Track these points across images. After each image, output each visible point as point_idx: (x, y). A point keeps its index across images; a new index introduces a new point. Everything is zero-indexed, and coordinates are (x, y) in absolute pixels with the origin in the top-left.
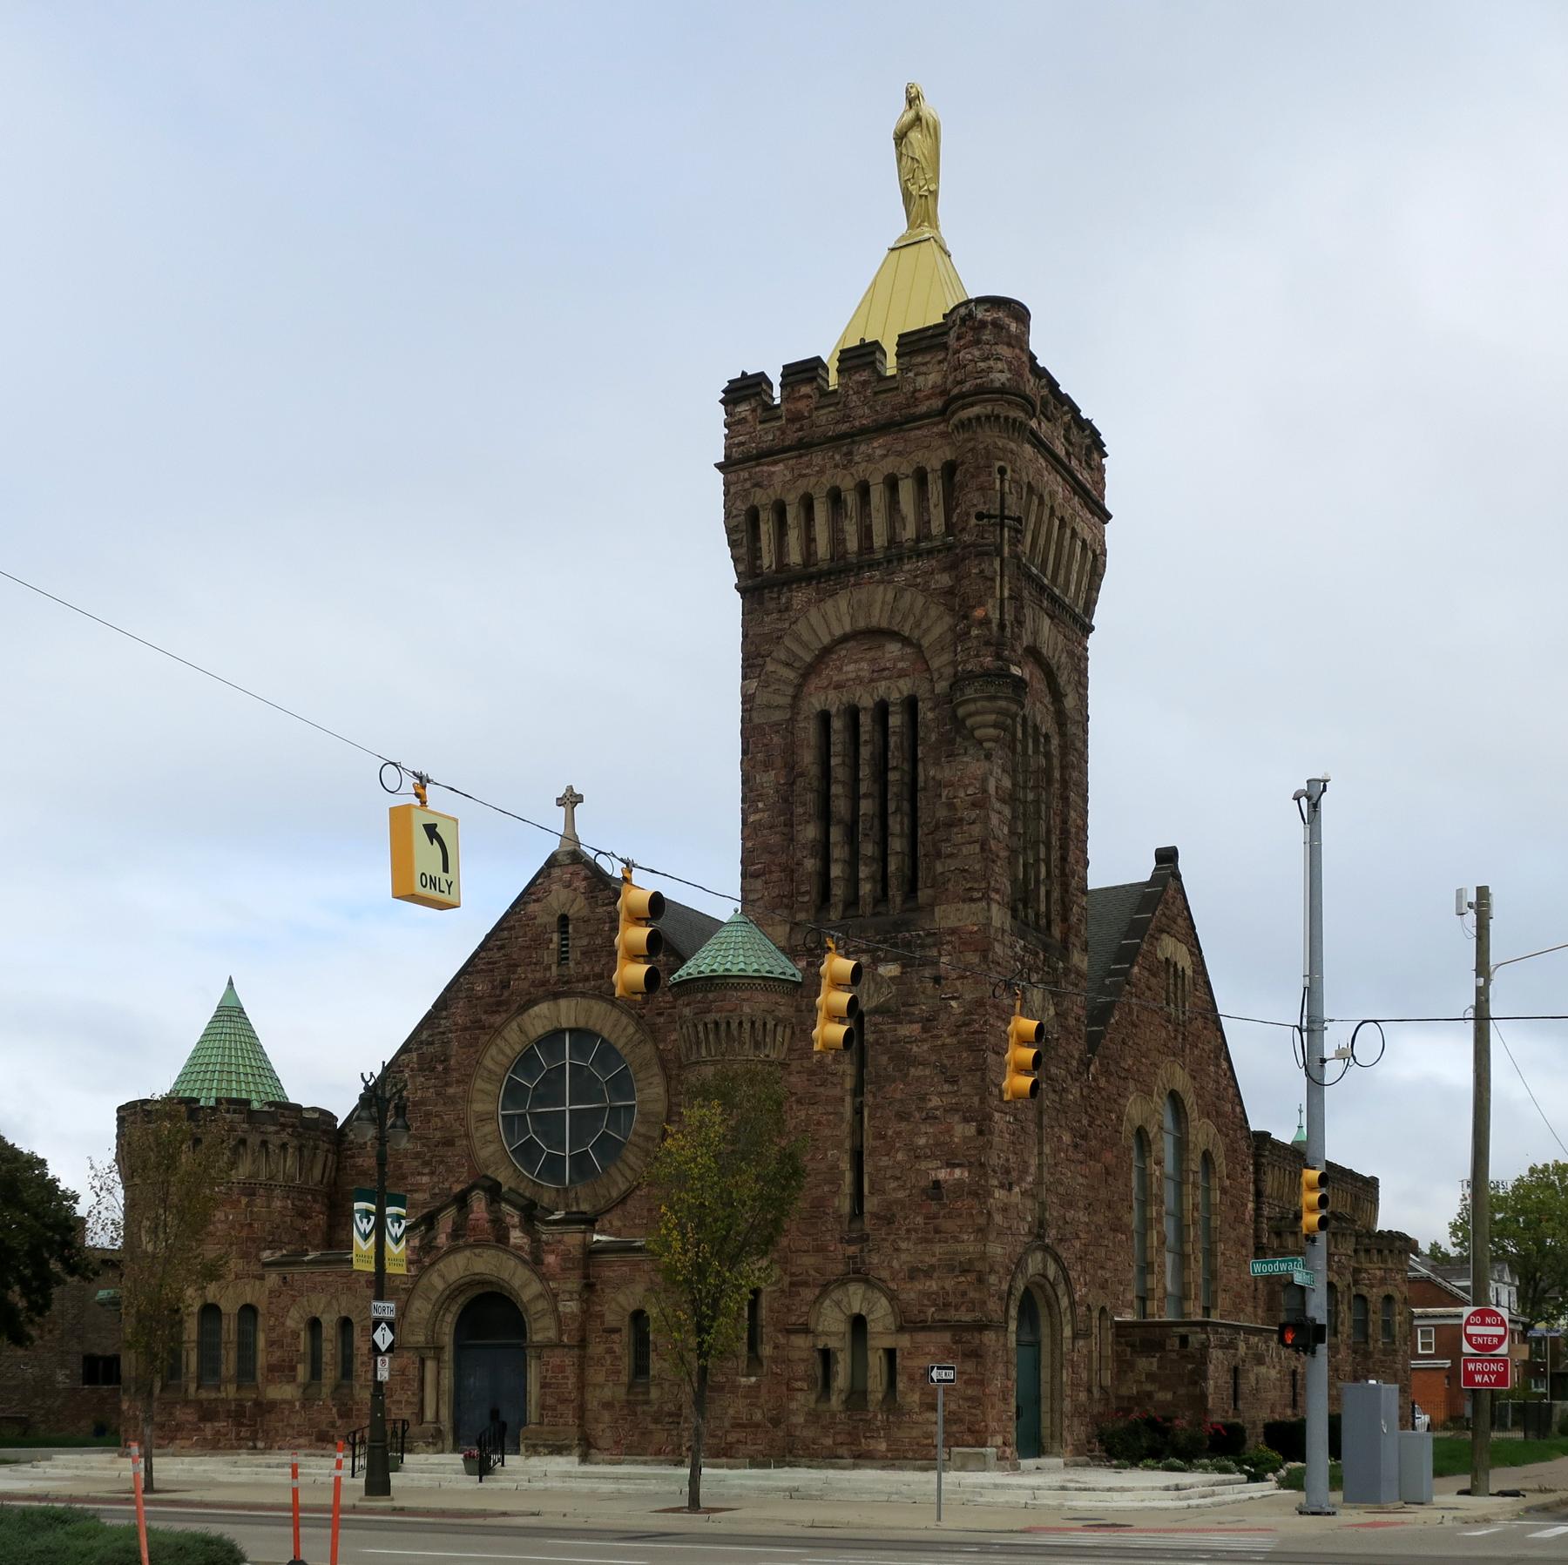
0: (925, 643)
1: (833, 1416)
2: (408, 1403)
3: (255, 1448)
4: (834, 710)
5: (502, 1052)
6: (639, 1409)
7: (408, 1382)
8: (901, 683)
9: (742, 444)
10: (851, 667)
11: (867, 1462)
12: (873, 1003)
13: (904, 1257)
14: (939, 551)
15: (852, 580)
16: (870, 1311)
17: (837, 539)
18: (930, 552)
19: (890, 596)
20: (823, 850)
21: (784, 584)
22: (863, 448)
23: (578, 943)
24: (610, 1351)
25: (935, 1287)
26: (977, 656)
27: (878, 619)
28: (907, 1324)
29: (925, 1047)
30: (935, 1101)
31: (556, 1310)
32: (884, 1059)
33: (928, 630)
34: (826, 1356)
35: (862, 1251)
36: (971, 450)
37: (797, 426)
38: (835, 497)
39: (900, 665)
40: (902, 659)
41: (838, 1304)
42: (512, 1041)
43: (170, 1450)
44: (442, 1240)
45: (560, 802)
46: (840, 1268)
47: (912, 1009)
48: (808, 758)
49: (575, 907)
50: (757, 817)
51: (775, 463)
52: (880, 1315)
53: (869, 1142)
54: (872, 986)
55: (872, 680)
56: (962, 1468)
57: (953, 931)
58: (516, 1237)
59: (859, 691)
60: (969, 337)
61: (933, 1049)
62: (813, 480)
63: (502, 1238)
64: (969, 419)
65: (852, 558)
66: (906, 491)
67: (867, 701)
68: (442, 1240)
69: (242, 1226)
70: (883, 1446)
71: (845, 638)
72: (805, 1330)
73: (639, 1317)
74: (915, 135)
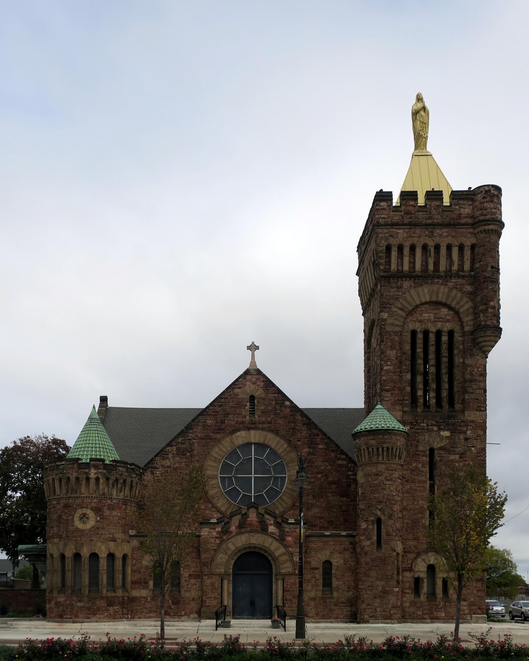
0: (461, 311)
1: (422, 603)
2: (215, 598)
3: (128, 618)
4: (419, 330)
5: (220, 449)
6: (328, 601)
7: (215, 589)
8: (447, 324)
9: (385, 218)
10: (426, 315)
11: (437, 621)
12: (439, 446)
14: (467, 277)
15: (430, 281)
17: (425, 264)
18: (463, 277)
19: (446, 290)
20: (413, 383)
21: (400, 277)
22: (438, 231)
23: (259, 408)
24: (314, 577)
26: (491, 320)
27: (442, 298)
32: (444, 467)
33: (463, 306)
34: (417, 581)
36: (488, 241)
37: (409, 216)
38: (425, 248)
39: (448, 317)
40: (448, 315)
41: (424, 560)
42: (226, 445)
43: (94, 619)
44: (233, 528)
45: (249, 348)
46: (425, 546)
47: (455, 449)
48: (407, 347)
50: (388, 367)
51: (399, 229)
54: (439, 439)
55: (435, 321)
56: (476, 622)
57: (473, 421)
58: (272, 529)
60: (488, 199)
61: (465, 465)
62: (416, 239)
63: (264, 529)
64: (489, 230)
66: (455, 252)
68: (233, 528)
69: (123, 518)
70: (443, 615)
72: (410, 570)
73: (327, 565)
74: (420, 115)
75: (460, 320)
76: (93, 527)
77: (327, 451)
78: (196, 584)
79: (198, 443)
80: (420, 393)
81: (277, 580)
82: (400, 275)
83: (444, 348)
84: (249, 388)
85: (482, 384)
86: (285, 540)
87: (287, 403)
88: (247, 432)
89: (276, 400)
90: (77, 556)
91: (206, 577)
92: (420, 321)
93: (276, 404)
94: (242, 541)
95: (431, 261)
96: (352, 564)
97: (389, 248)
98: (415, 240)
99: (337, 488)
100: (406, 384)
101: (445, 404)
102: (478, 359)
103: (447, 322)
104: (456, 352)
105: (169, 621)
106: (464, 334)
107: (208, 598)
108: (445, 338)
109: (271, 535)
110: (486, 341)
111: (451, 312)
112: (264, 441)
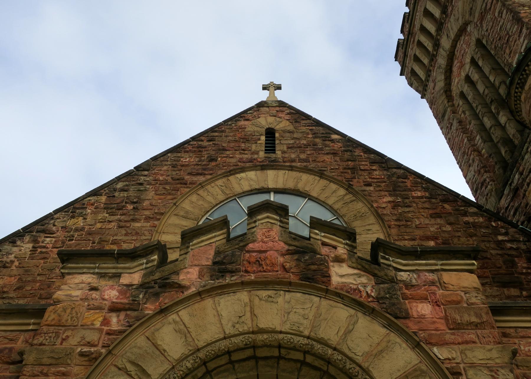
86: (407, 317)
87: (335, 137)
88: (259, 172)
109: (347, 297)
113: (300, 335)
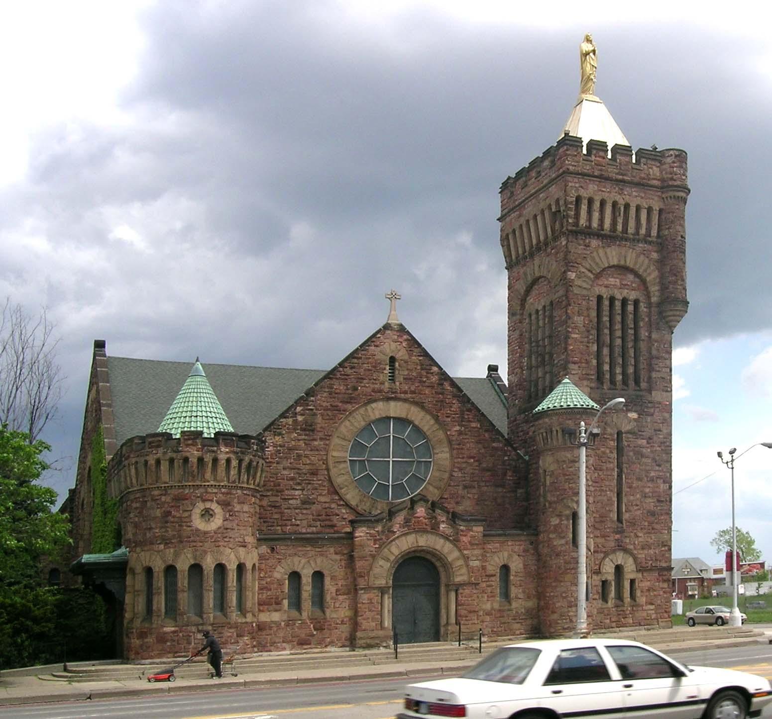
0: (648, 279)
4: (605, 297)
5: (352, 424)
13: (640, 539)
15: (618, 243)
16: (625, 563)
17: (614, 223)
19: (634, 255)
22: (628, 189)
25: (652, 553)
27: (630, 263)
28: (641, 569)
29: (649, 450)
30: (653, 474)
31: (467, 566)
32: (631, 454)
34: (604, 583)
35: (621, 537)
38: (615, 205)
42: (357, 420)
49: (400, 354)
52: (629, 566)
53: (625, 489)
55: (621, 288)
59: (616, 291)
61: (652, 451)
64: (678, 197)
65: (641, 237)
67: (619, 296)
71: (613, 266)
73: (505, 569)
75: (646, 288)
76: (219, 528)
77: (481, 431)
78: (345, 602)
79: (322, 415)
80: (606, 367)
81: (448, 592)
82: (588, 232)
83: (630, 318)
84: (390, 347)
85: (667, 362)
87: (435, 369)
89: (422, 365)
90: (196, 569)
91: (363, 592)
92: (606, 287)
93: (422, 369)
94: (404, 544)
95: (620, 220)
96: (533, 568)
97: (578, 200)
98: (606, 196)
99: (491, 476)
100: (592, 357)
101: (631, 383)
102: (664, 334)
103: (633, 290)
104: (641, 324)
105: (403, 648)
106: (649, 305)
107: (364, 619)
108: (630, 308)
110: (674, 316)
111: (637, 280)
112: (407, 415)
113: (430, 547)
